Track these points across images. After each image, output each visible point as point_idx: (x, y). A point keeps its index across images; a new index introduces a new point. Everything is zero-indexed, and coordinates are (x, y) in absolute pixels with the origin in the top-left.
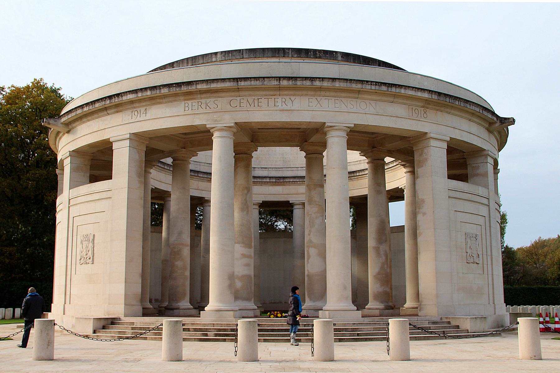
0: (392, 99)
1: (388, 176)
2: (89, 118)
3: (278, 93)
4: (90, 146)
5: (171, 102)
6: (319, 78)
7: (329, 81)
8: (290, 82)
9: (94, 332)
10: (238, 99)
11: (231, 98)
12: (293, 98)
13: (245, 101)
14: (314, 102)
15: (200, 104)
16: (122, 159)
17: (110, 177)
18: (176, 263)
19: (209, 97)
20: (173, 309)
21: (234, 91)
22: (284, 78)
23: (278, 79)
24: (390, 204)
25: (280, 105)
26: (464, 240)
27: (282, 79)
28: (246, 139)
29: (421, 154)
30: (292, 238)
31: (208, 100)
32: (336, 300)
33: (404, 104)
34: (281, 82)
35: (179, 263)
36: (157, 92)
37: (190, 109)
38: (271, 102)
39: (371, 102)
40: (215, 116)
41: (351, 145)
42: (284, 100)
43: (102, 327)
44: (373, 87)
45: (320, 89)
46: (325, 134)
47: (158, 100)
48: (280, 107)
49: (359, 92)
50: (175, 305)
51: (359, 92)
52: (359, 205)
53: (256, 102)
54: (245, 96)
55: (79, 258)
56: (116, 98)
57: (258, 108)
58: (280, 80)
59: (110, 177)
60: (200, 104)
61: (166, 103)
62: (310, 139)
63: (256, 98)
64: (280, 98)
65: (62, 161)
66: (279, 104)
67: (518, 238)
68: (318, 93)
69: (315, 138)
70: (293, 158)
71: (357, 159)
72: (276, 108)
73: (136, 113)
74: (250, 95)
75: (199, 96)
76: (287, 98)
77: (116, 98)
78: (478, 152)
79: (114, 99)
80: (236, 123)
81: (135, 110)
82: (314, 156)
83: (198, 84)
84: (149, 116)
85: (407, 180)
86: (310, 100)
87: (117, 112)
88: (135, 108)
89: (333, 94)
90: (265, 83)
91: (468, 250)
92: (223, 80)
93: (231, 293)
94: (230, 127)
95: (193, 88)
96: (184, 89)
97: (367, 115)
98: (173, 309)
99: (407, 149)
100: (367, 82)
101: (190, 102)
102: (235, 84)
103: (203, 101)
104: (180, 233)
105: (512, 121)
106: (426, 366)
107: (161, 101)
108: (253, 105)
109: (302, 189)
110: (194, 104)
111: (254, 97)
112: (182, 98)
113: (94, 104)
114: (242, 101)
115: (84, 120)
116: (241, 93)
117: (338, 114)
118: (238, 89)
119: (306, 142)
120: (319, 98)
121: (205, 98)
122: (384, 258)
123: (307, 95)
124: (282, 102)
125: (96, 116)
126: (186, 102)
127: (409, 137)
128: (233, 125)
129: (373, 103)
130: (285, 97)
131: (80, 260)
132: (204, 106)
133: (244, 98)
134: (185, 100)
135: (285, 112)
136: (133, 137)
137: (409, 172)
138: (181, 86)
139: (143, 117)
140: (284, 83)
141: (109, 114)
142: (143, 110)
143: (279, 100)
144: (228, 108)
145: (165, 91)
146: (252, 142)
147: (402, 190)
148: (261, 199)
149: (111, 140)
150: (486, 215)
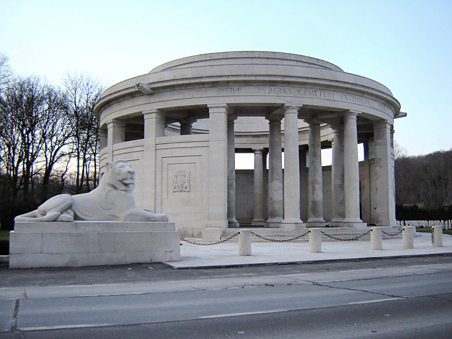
1: (323, 132)
12: (334, 93)
13: (308, 92)
15: (280, 90)
17: (143, 137)
19: (286, 86)
24: (235, 154)
31: (285, 88)
38: (322, 94)
41: (299, 117)
46: (284, 110)
47: (250, 84)
52: (303, 150)
53: (314, 93)
54: (308, 88)
57: (315, 97)
59: (143, 137)
60: (280, 90)
62: (273, 113)
63: (314, 90)
64: (327, 92)
65: (105, 125)
66: (326, 95)
69: (277, 112)
70: (261, 124)
71: (303, 124)
73: (230, 90)
74: (311, 88)
76: (331, 92)
78: (382, 122)
82: (275, 124)
85: (310, 136)
87: (213, 87)
99: (338, 119)
101: (273, 88)
106: (222, 250)
114: (306, 91)
116: (307, 86)
117: (293, 99)
120: (346, 95)
121: (283, 86)
132: (282, 91)
134: (269, 86)
139: (236, 93)
142: (236, 88)
143: (327, 93)
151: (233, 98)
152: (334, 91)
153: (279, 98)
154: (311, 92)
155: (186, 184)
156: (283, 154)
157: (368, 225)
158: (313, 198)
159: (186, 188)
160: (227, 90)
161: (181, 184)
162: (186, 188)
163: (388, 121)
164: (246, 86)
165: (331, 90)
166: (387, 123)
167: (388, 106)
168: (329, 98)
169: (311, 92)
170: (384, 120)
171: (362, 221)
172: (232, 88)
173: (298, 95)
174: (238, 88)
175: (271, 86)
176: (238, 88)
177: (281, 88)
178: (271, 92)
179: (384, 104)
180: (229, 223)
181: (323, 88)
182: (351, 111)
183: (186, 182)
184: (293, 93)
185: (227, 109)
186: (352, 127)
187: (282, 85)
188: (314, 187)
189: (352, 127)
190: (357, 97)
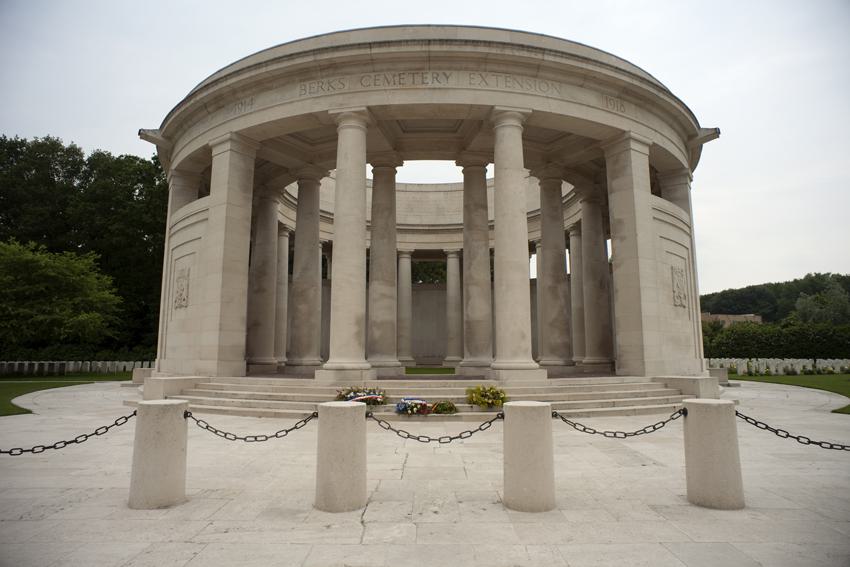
2: (190, 123)
5: (283, 85)
10: (372, 75)
12: (448, 73)
13: (382, 78)
14: (477, 79)
19: (333, 75)
26: (670, 276)
28: (386, 145)
30: (446, 289)
32: (346, 355)
33: (596, 90)
40: (340, 99)
42: (435, 75)
48: (430, 85)
50: (296, 360)
51: (538, 67)
53: (397, 78)
54: (382, 71)
64: (430, 73)
67: (710, 283)
68: (483, 67)
72: (424, 86)
74: (389, 70)
75: (319, 74)
80: (369, 108)
84: (256, 107)
88: (238, 99)
93: (360, 344)
97: (550, 101)
103: (325, 80)
109: (459, 237)
111: (393, 72)
116: (378, 67)
119: (464, 149)
120: (484, 74)
121: (327, 76)
122: (563, 300)
123: (466, 69)
127: (600, 141)
128: (364, 108)
129: (557, 85)
132: (325, 87)
134: (301, 81)
135: (437, 91)
136: (235, 137)
137: (584, 200)
139: (248, 109)
141: (209, 113)
142: (248, 100)
143: (429, 76)
146: (395, 149)
148: (412, 248)
150: (689, 246)
151: (242, 119)
152: (449, 69)
153: (317, 101)
154: (390, 77)
156: (534, 275)
157: (550, 376)
164: (262, 91)
165: (440, 69)
166: (630, 138)
168: (437, 85)
169: (390, 77)
170: (624, 132)
171: (537, 365)
173: (359, 87)
175: (304, 81)
180: (248, 364)
181: (418, 66)
184: (347, 85)
186: (511, 142)
187: (324, 74)
188: (467, 291)
189: (511, 142)
190: (519, 78)
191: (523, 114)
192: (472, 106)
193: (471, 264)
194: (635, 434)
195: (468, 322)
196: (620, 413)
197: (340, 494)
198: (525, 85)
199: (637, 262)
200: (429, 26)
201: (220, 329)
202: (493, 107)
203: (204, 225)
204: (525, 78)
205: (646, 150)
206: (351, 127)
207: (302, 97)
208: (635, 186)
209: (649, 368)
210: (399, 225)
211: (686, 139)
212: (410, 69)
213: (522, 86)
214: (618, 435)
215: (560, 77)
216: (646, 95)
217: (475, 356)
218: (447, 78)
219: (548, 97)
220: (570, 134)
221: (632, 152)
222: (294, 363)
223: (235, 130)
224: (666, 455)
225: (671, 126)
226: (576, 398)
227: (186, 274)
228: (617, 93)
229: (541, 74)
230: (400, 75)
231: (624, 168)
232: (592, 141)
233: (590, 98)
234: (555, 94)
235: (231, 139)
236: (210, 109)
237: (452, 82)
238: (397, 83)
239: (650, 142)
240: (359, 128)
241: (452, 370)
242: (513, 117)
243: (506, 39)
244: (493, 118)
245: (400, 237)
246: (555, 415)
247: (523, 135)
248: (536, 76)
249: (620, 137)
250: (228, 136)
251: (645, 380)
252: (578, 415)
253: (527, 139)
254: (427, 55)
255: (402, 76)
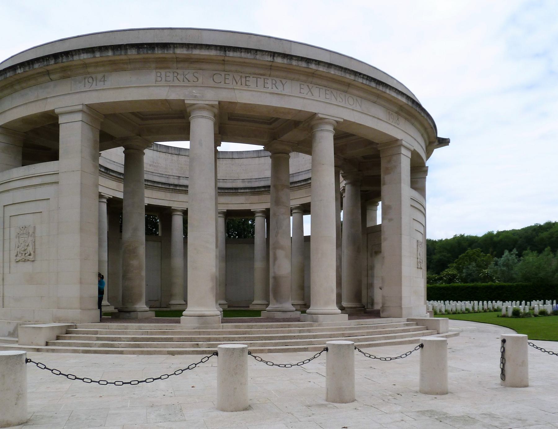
0: (375, 99)
2: (24, 85)
3: (269, 73)
4: (25, 120)
6: (316, 61)
7: (324, 66)
8: (285, 61)
9: (47, 344)
10: (223, 73)
11: (215, 72)
13: (231, 77)
14: (305, 90)
16: (74, 136)
17: (54, 156)
18: (131, 262)
20: (129, 312)
21: (218, 63)
22: (279, 54)
23: (272, 54)
25: (270, 88)
27: (276, 55)
29: (389, 161)
31: (186, 72)
34: (275, 58)
35: (134, 263)
36: (121, 56)
37: (164, 79)
39: (358, 99)
42: (274, 82)
43: (55, 338)
44: (365, 81)
45: (313, 74)
48: (270, 90)
49: (349, 85)
51: (349, 85)
53: (243, 80)
55: (13, 253)
56: (64, 57)
58: (274, 56)
60: (176, 74)
61: (132, 69)
63: (243, 75)
66: (269, 85)
68: (310, 79)
72: (265, 90)
73: (90, 80)
74: (236, 71)
75: (175, 65)
76: (278, 80)
77: (64, 57)
79: (60, 59)
81: (89, 76)
83: (177, 47)
84: (108, 84)
86: (302, 86)
87: (64, 78)
88: (89, 73)
89: (325, 83)
90: (258, 57)
91: (419, 257)
92: (208, 47)
94: (213, 106)
95: (168, 53)
96: (158, 53)
97: (355, 112)
98: (129, 312)
100: (360, 74)
101: (163, 72)
102: (222, 53)
103: (179, 71)
104: (136, 230)
105: (444, 142)
107: (126, 66)
108: (239, 83)
110: (168, 74)
111: (241, 74)
112: (153, 65)
113: (33, 64)
115: (17, 87)
118: (224, 62)
120: (310, 86)
123: (298, 80)
124: (272, 84)
125: (32, 82)
126: (158, 70)
129: (359, 99)
130: (275, 78)
131: (16, 256)
132: (180, 77)
133: (229, 73)
134: (156, 68)
136: (85, 109)
138: (154, 48)
139: (100, 85)
140: (279, 60)
141: (52, 80)
142: (100, 76)
143: (269, 81)
144: (211, 83)
145: (132, 53)
147: (229, 215)
149: (57, 111)
154: (238, 78)
155: (30, 249)
158: (274, 272)
159: (30, 255)
160: (86, 80)
161: (23, 249)
162: (30, 255)
163: (404, 143)
164: (116, 70)
165: (277, 77)
167: (406, 119)
168: (275, 90)
169: (238, 78)
172: (94, 76)
174: (104, 76)
175: (161, 68)
176: (104, 76)
177: (178, 71)
178: (159, 79)
179: (396, 113)
181: (262, 72)
182: (320, 116)
183: (30, 245)
185: (271, 157)
186: (326, 143)
187: (180, 65)
188: (275, 254)
190: (334, 92)
191: (337, 122)
192: (300, 111)
193: (277, 233)
194: (396, 358)
195: (275, 278)
196: (142, 353)
197: (340, 394)
198: (339, 99)
199: (401, 237)
200: (269, 37)
201: (81, 283)
202: (315, 114)
203: (54, 187)
204: (339, 92)
205: (409, 155)
206: (203, 117)
207: (158, 84)
208: (402, 181)
209: (404, 312)
210: (154, 185)
211: (428, 143)
212: (255, 74)
213: (361, 106)
214: (405, 356)
215: (362, 94)
216: (412, 111)
217: (281, 303)
218: (283, 85)
219: (353, 110)
220: (354, 135)
221: (402, 155)
222: (129, 310)
223: (87, 103)
224: (408, 370)
225: (422, 135)
226: (372, 333)
227: (31, 232)
228: (396, 109)
229: (350, 90)
230: (246, 77)
231: (395, 168)
232: (369, 143)
233: (379, 112)
234: (358, 108)
235: (81, 111)
236: (52, 77)
237: (287, 91)
238: (244, 84)
239: (412, 149)
240: (210, 119)
241: (257, 313)
242: (330, 123)
243: (326, 58)
244: (313, 122)
245: (100, 187)
246: (250, 353)
247: (334, 136)
248: (346, 92)
249: (394, 144)
250: (80, 107)
251: (403, 320)
252: (262, 351)
253: (336, 138)
254: (270, 64)
255: (247, 79)
